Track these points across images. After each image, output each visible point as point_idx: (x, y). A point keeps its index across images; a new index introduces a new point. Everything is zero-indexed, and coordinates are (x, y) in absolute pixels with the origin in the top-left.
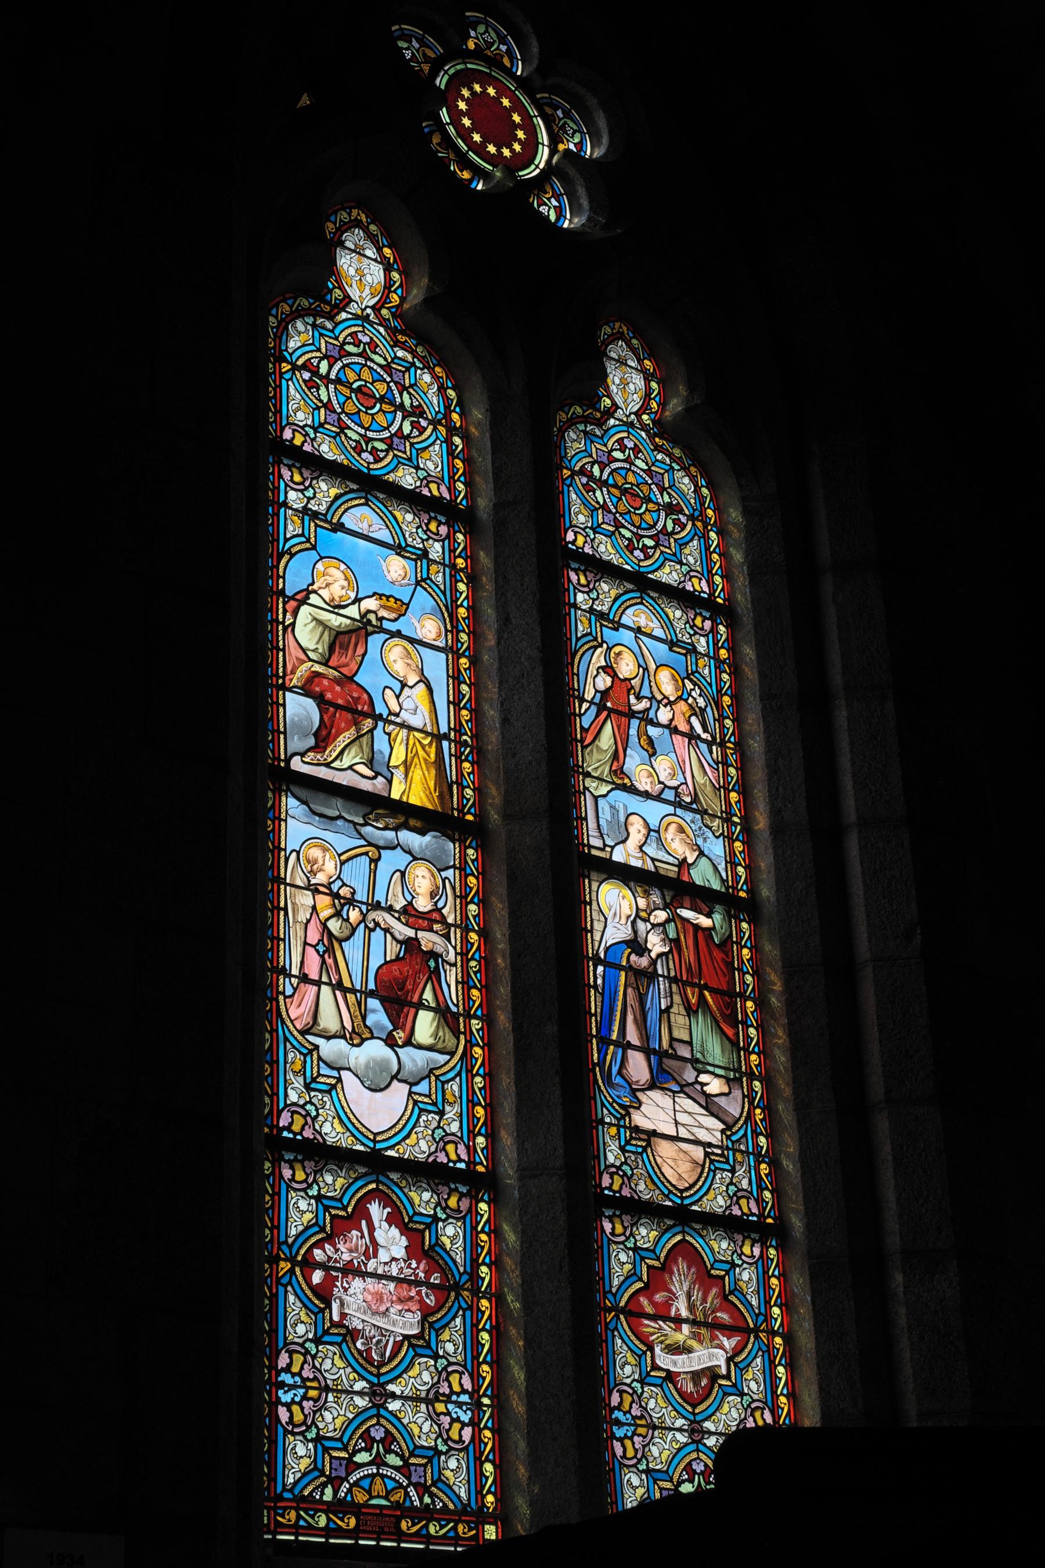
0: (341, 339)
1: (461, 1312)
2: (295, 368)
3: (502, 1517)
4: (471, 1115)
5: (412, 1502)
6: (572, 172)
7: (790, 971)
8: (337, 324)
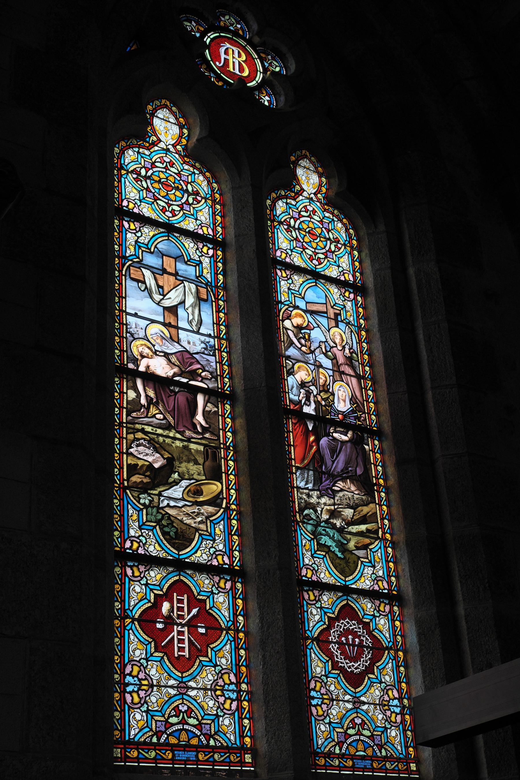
0: (299, 209)
2: (128, 172)
3: (253, 751)
4: (388, 568)
5: (376, 753)
6: (276, 83)
7: (399, 464)
8: (297, 202)
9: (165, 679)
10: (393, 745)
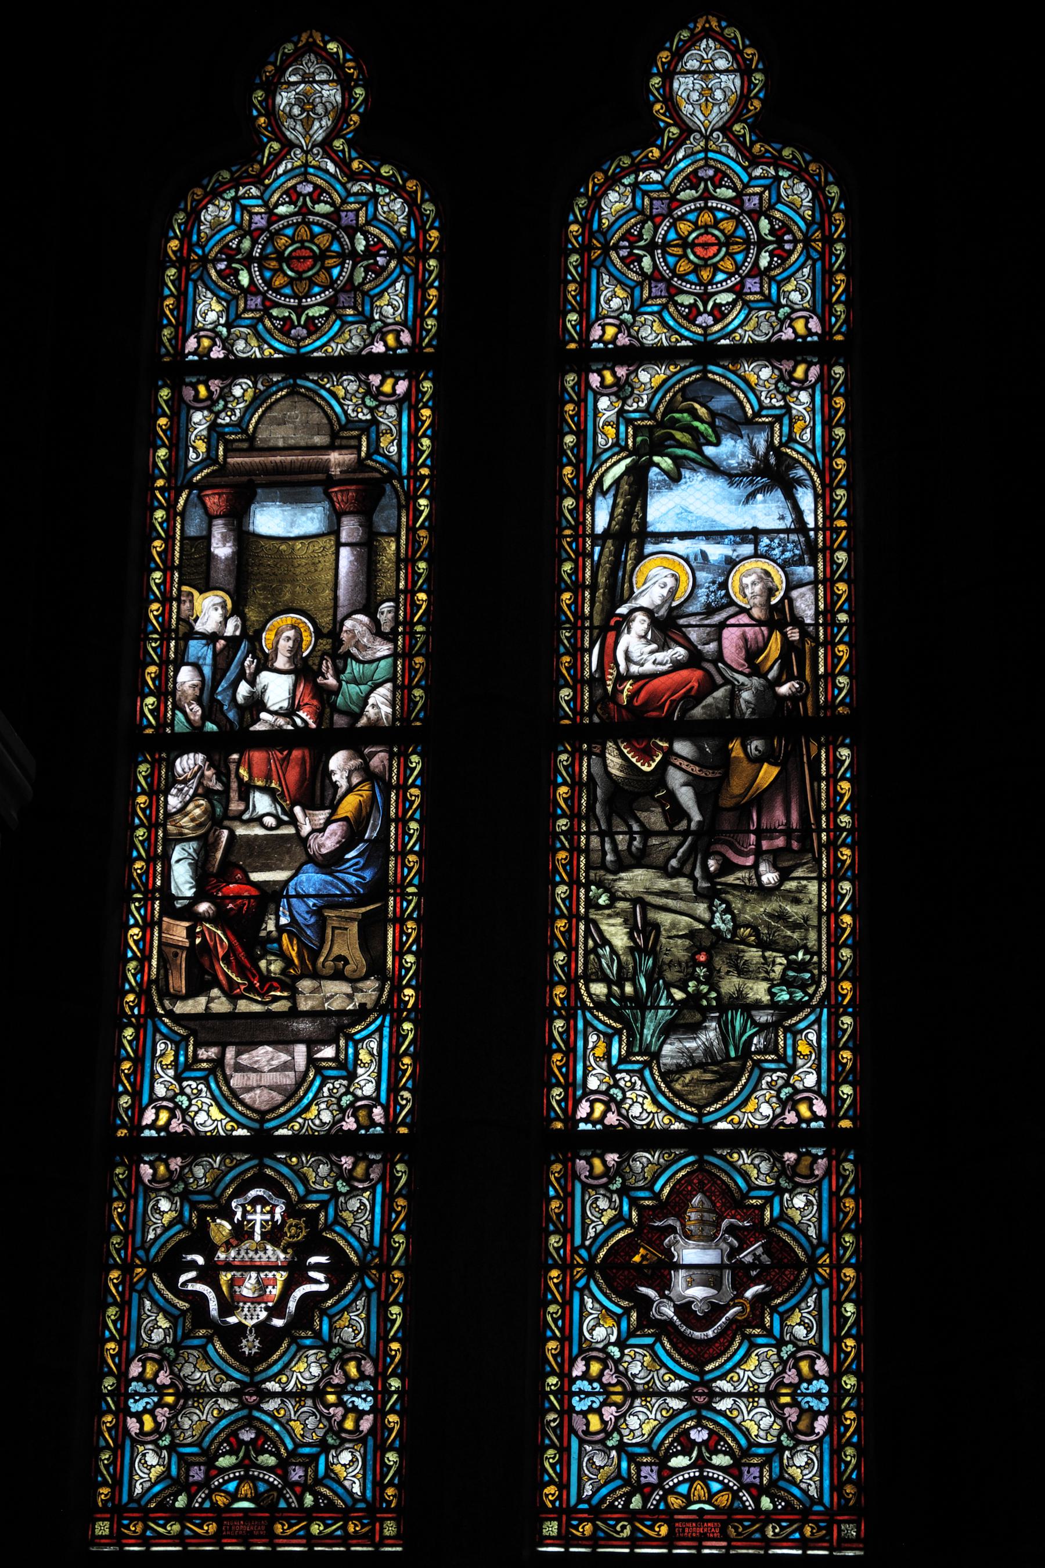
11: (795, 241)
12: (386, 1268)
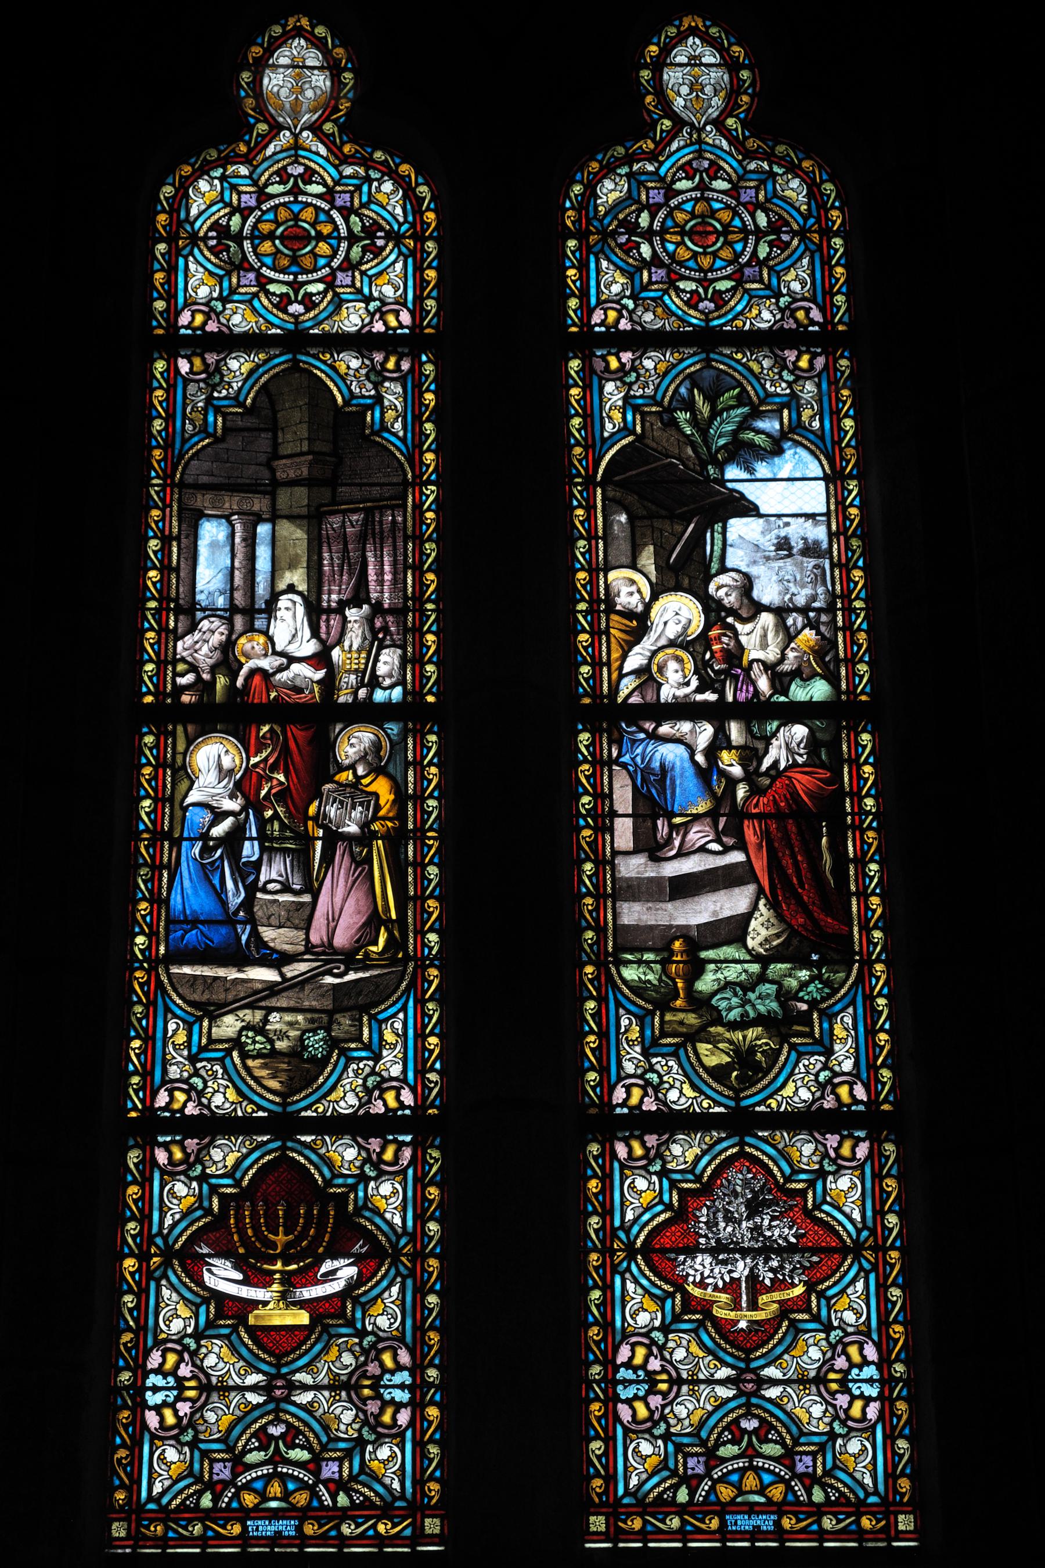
1: (399, 1279)
9: (239, 1375)
10: (851, 1475)
11: (205, 238)
12: (880, 1249)
